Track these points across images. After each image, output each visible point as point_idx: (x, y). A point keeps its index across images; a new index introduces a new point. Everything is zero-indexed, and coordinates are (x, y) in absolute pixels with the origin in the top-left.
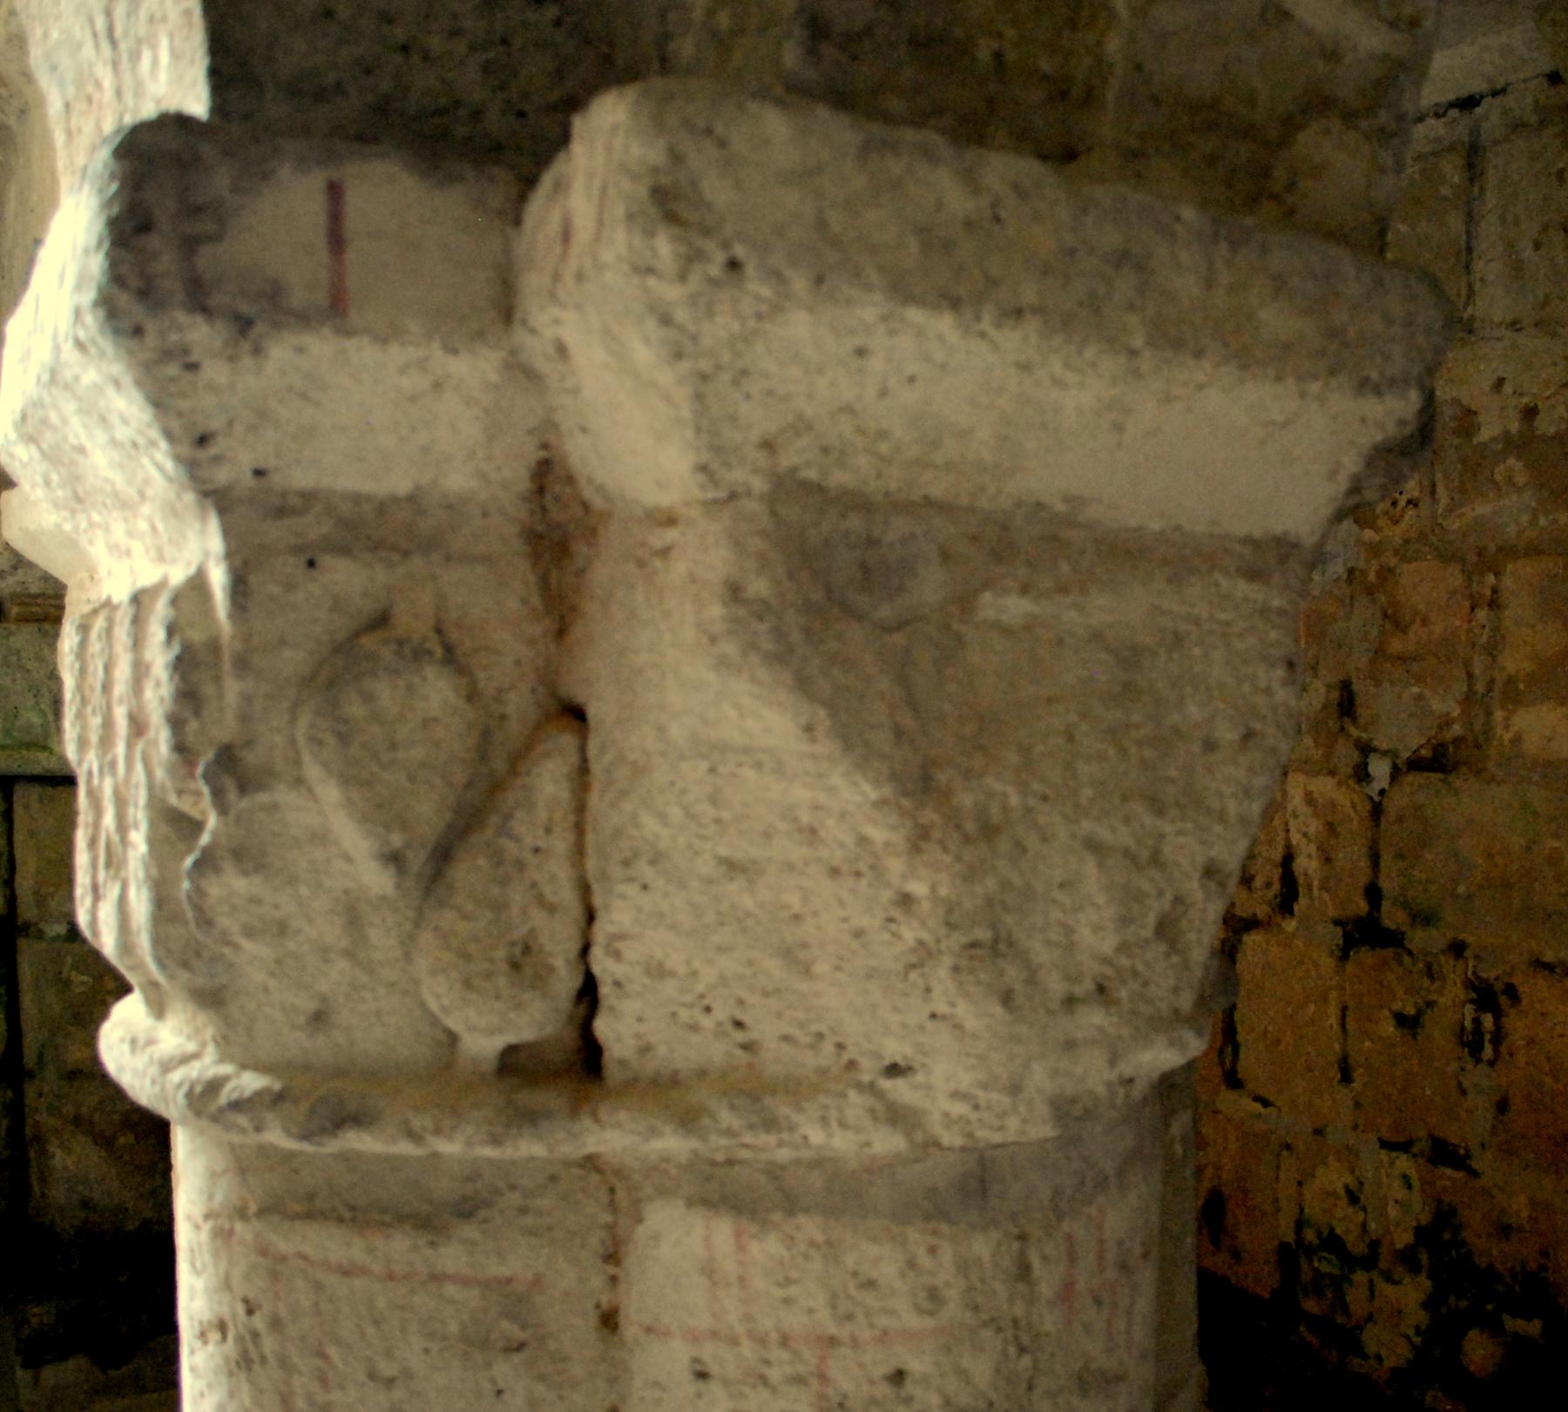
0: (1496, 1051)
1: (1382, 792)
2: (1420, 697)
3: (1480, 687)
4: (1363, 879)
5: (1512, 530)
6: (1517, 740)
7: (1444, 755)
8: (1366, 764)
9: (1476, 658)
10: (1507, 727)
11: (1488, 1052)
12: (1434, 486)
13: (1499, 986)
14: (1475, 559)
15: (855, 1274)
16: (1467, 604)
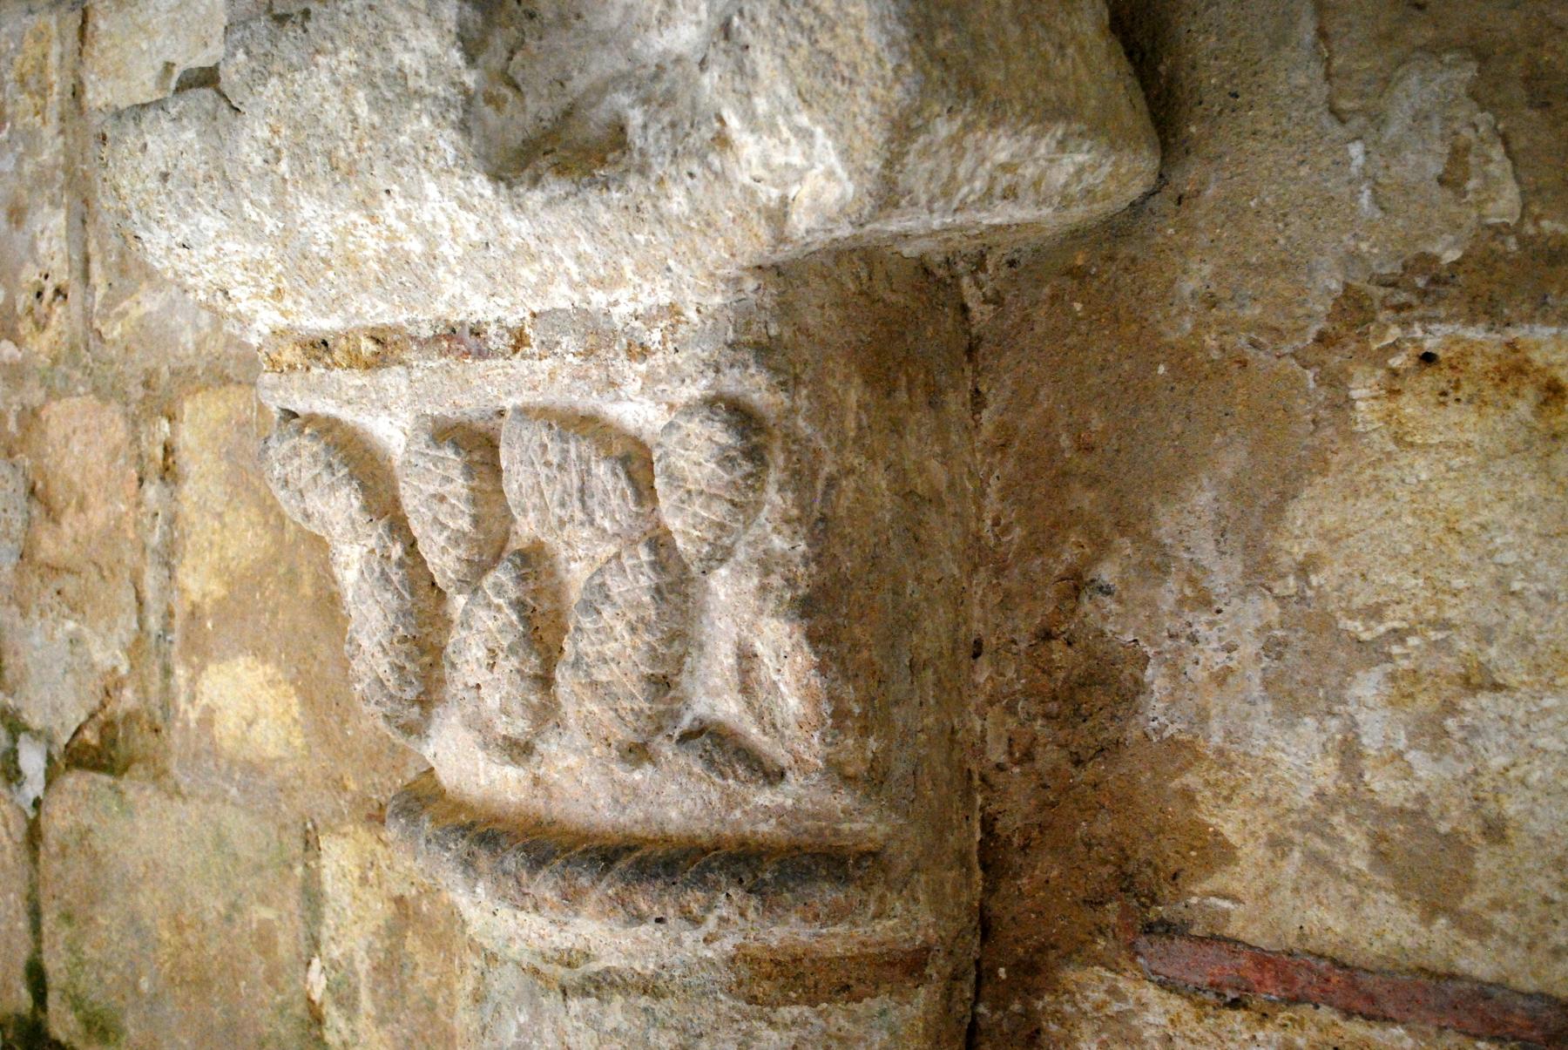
1: (37, 803)
2: (75, 641)
3: (154, 623)
4: (23, 954)
5: (188, 338)
7: (114, 742)
8: (15, 752)
9: (147, 569)
10: (192, 699)
12: (87, 260)
14: (139, 393)
16: (133, 473)
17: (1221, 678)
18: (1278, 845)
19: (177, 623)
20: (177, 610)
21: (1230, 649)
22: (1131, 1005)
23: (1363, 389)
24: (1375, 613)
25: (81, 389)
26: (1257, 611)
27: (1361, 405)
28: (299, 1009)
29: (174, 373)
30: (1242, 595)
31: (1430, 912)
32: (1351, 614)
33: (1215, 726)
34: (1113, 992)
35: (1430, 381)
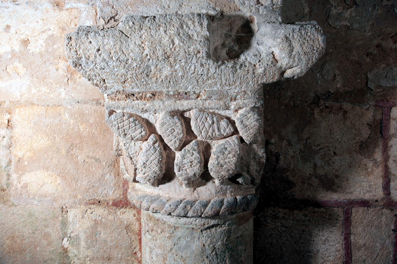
6: (25, 186)
17: (293, 157)
18: (303, 183)
19: (13, 164)
20: (12, 160)
23: (316, 111)
24: (319, 145)
27: (316, 114)
29: (10, 102)
32: (315, 146)
33: (292, 164)
34: (274, 211)
35: (327, 110)
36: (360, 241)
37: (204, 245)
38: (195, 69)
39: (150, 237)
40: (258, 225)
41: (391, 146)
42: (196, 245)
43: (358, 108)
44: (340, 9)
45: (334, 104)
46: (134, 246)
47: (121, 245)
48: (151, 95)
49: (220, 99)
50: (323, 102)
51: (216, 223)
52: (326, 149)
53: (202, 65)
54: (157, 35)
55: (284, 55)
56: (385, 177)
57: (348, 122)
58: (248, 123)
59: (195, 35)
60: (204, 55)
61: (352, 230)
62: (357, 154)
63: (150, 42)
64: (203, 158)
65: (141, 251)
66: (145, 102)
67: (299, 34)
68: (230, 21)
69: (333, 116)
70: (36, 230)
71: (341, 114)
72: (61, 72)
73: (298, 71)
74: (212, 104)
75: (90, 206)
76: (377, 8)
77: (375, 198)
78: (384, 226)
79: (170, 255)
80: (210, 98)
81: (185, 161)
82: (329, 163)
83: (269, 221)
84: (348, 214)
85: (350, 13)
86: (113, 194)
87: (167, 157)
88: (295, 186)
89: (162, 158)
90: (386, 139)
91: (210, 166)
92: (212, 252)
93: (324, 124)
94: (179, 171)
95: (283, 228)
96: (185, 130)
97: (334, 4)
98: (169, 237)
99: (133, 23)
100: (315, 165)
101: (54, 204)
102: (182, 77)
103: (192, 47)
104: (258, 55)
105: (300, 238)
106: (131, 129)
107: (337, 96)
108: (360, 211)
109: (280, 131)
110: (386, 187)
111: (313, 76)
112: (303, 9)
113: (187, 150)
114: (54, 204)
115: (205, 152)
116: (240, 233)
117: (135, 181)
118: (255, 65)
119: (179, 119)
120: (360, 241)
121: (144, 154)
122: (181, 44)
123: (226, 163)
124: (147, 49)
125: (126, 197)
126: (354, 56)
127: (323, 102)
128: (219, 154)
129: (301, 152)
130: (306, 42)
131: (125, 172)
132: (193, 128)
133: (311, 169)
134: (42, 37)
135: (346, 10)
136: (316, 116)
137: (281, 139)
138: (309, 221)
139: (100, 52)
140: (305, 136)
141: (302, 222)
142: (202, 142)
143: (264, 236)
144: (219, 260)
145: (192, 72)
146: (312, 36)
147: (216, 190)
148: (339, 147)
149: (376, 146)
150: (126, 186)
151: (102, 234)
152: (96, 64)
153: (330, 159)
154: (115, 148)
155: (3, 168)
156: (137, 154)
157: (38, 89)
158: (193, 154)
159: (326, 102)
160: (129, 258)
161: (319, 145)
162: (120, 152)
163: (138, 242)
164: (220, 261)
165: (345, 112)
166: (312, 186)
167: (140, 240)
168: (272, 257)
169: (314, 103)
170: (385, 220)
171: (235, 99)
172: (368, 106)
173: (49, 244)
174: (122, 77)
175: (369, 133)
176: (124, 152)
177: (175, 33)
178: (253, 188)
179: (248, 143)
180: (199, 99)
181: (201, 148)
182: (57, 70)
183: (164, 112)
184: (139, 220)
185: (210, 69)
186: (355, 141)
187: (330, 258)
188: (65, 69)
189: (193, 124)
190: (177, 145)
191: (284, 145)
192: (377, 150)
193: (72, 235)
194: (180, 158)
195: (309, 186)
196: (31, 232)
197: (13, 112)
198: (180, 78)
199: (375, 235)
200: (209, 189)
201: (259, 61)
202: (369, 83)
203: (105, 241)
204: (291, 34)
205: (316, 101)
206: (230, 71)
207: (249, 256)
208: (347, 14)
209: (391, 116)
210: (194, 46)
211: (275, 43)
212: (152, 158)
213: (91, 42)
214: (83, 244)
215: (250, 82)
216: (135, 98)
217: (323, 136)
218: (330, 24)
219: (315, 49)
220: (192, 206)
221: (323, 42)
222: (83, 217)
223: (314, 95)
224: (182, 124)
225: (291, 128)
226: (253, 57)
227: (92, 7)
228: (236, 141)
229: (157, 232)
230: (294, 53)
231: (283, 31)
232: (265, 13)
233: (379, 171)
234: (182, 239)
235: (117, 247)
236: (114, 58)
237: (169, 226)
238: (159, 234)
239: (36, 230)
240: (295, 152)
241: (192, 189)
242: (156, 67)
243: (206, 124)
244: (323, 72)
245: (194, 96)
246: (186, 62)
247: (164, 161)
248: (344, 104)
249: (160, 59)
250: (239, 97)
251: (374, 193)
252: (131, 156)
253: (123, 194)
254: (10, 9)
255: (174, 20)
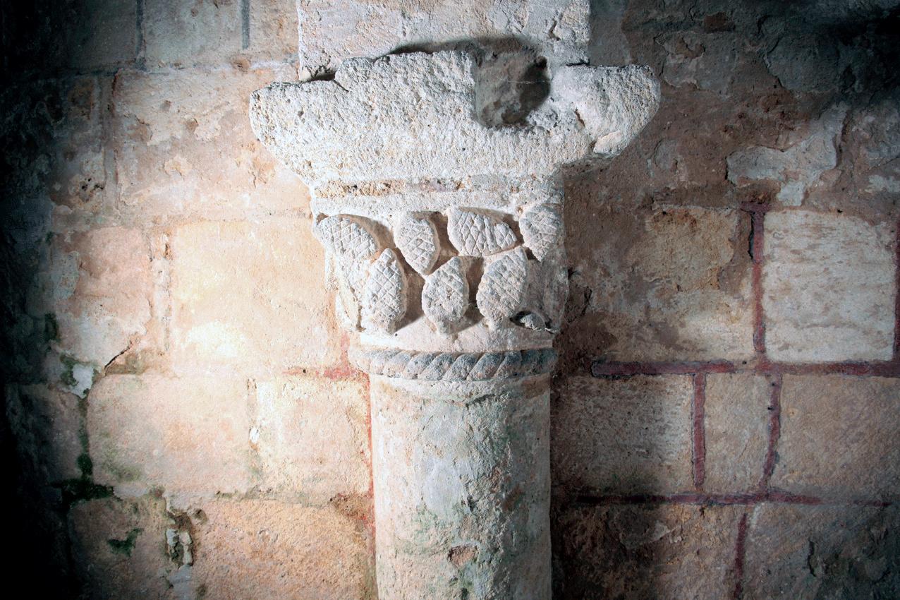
0: (193, 556)
1: (86, 392)
3: (160, 313)
6: (193, 347)
8: (71, 373)
10: (183, 341)
11: (187, 558)
13: (191, 513)
15: (424, 551)
17: (612, 295)
19: (174, 313)
21: (615, 287)
22: (587, 384)
23: (648, 221)
24: (653, 275)
25: (114, 224)
26: (622, 277)
28: (247, 447)
29: (170, 218)
30: (618, 273)
31: (668, 347)
32: (647, 276)
33: (611, 306)
34: (583, 382)
35: (666, 218)
36: (719, 427)
37: (471, 428)
38: (453, 139)
39: (385, 420)
40: (556, 402)
41: (766, 275)
42: (458, 429)
43: (713, 215)
44: (680, 59)
45: (676, 207)
46: (360, 441)
47: (339, 440)
48: (384, 187)
49: (494, 190)
50: (658, 206)
51: (491, 393)
52: (664, 281)
53: (464, 133)
54: (392, 86)
55: (594, 113)
56: (757, 324)
57: (698, 237)
58: (540, 231)
59: (453, 84)
60: (467, 115)
61: (706, 411)
62: (714, 288)
63: (382, 97)
64: (467, 286)
65: (371, 450)
66: (373, 198)
67: (618, 78)
68: (507, 66)
69: (674, 228)
70: (209, 415)
71: (687, 225)
72: (244, 168)
73: (618, 140)
74: (483, 200)
75: (291, 377)
76: (737, 57)
77: (743, 358)
78: (755, 402)
79: (417, 444)
80: (477, 187)
81: (439, 289)
82: (670, 303)
83: (575, 398)
84: (700, 385)
85: (696, 63)
86: (325, 358)
87: (410, 286)
88: (617, 342)
89: (402, 285)
90: (759, 263)
91: (478, 297)
92: (485, 438)
93: (660, 240)
94: (430, 306)
95: (598, 410)
96: (438, 240)
97: (670, 51)
98: (416, 417)
99: (355, 69)
100: (648, 308)
101: (236, 375)
102: (433, 153)
103: (448, 103)
104: (553, 115)
105: (625, 425)
106: (352, 241)
107: (680, 196)
108: (720, 379)
109: (591, 253)
110: (759, 341)
111: (641, 163)
112: (623, 58)
113: (441, 273)
114: (236, 375)
115: (473, 273)
116: (529, 411)
117: (359, 328)
118: (548, 132)
119: (429, 224)
120: (719, 427)
121: (371, 279)
122: (430, 98)
123: (505, 291)
124: (377, 108)
125: (347, 363)
126: (706, 131)
127: (658, 206)
128: (493, 278)
129: (625, 285)
130: (629, 91)
131: (344, 316)
132: (452, 239)
133: (642, 314)
134: (215, 116)
135: (689, 59)
136: (648, 227)
137: (593, 265)
138: (639, 397)
139: (303, 116)
140: (631, 260)
141: (629, 398)
142: (466, 258)
143: (567, 422)
144: (495, 452)
145: (447, 144)
146: (638, 81)
147: (490, 339)
148: (686, 277)
149: (743, 275)
150: (345, 345)
151: (310, 422)
152: (297, 135)
153: (671, 297)
154: (327, 276)
155: (160, 319)
156: (362, 283)
157: (210, 195)
158: (452, 278)
159: (664, 206)
160: (353, 459)
161: (653, 275)
162: (335, 283)
163: (367, 435)
164: (498, 453)
165: (695, 221)
166: (644, 340)
167: (370, 430)
168: (580, 456)
169: (644, 207)
170: (757, 392)
171: (518, 190)
172: (729, 210)
173: (229, 438)
174: (337, 156)
175: (732, 253)
176: (342, 283)
177: (421, 81)
178: (549, 338)
179: (539, 259)
180: (460, 190)
181: (465, 269)
182: (238, 165)
183: (404, 213)
184: (367, 399)
185: (477, 138)
186: (710, 267)
187: (672, 455)
188: (250, 162)
189: (450, 230)
190: (426, 264)
191: (597, 275)
192: (744, 281)
193: (264, 423)
194: (431, 285)
195: (639, 342)
196: (202, 417)
197: (173, 232)
198: (430, 156)
199: (741, 417)
200: (478, 338)
201: (555, 125)
202: (729, 173)
203: (315, 434)
204: (605, 79)
205: (648, 202)
206: (508, 142)
207: (543, 449)
208: (692, 65)
209: (765, 227)
210: (451, 101)
211: (580, 95)
212: (385, 287)
213: (289, 101)
214: (281, 437)
215: (542, 159)
216: (358, 192)
217: (660, 259)
218: (665, 82)
219: (644, 102)
220: (451, 363)
221: (657, 91)
222: (280, 395)
223: (643, 194)
224: (433, 231)
225: (607, 248)
226: (545, 119)
227: (292, 66)
228: (521, 255)
229: (395, 409)
230: (610, 108)
231: (592, 76)
232: (562, 51)
233: (748, 315)
234: (435, 419)
235: (333, 442)
236: (324, 124)
237: (415, 399)
238: (399, 413)
239: (209, 415)
240: (615, 287)
241: (451, 338)
242: (391, 138)
243: (472, 229)
244: (658, 157)
245: (453, 186)
246: (438, 128)
247: (405, 292)
248: (692, 207)
249: (397, 124)
250: (523, 185)
251: (740, 350)
252: (354, 286)
253: (341, 358)
254: (171, 78)
255: (419, 62)
